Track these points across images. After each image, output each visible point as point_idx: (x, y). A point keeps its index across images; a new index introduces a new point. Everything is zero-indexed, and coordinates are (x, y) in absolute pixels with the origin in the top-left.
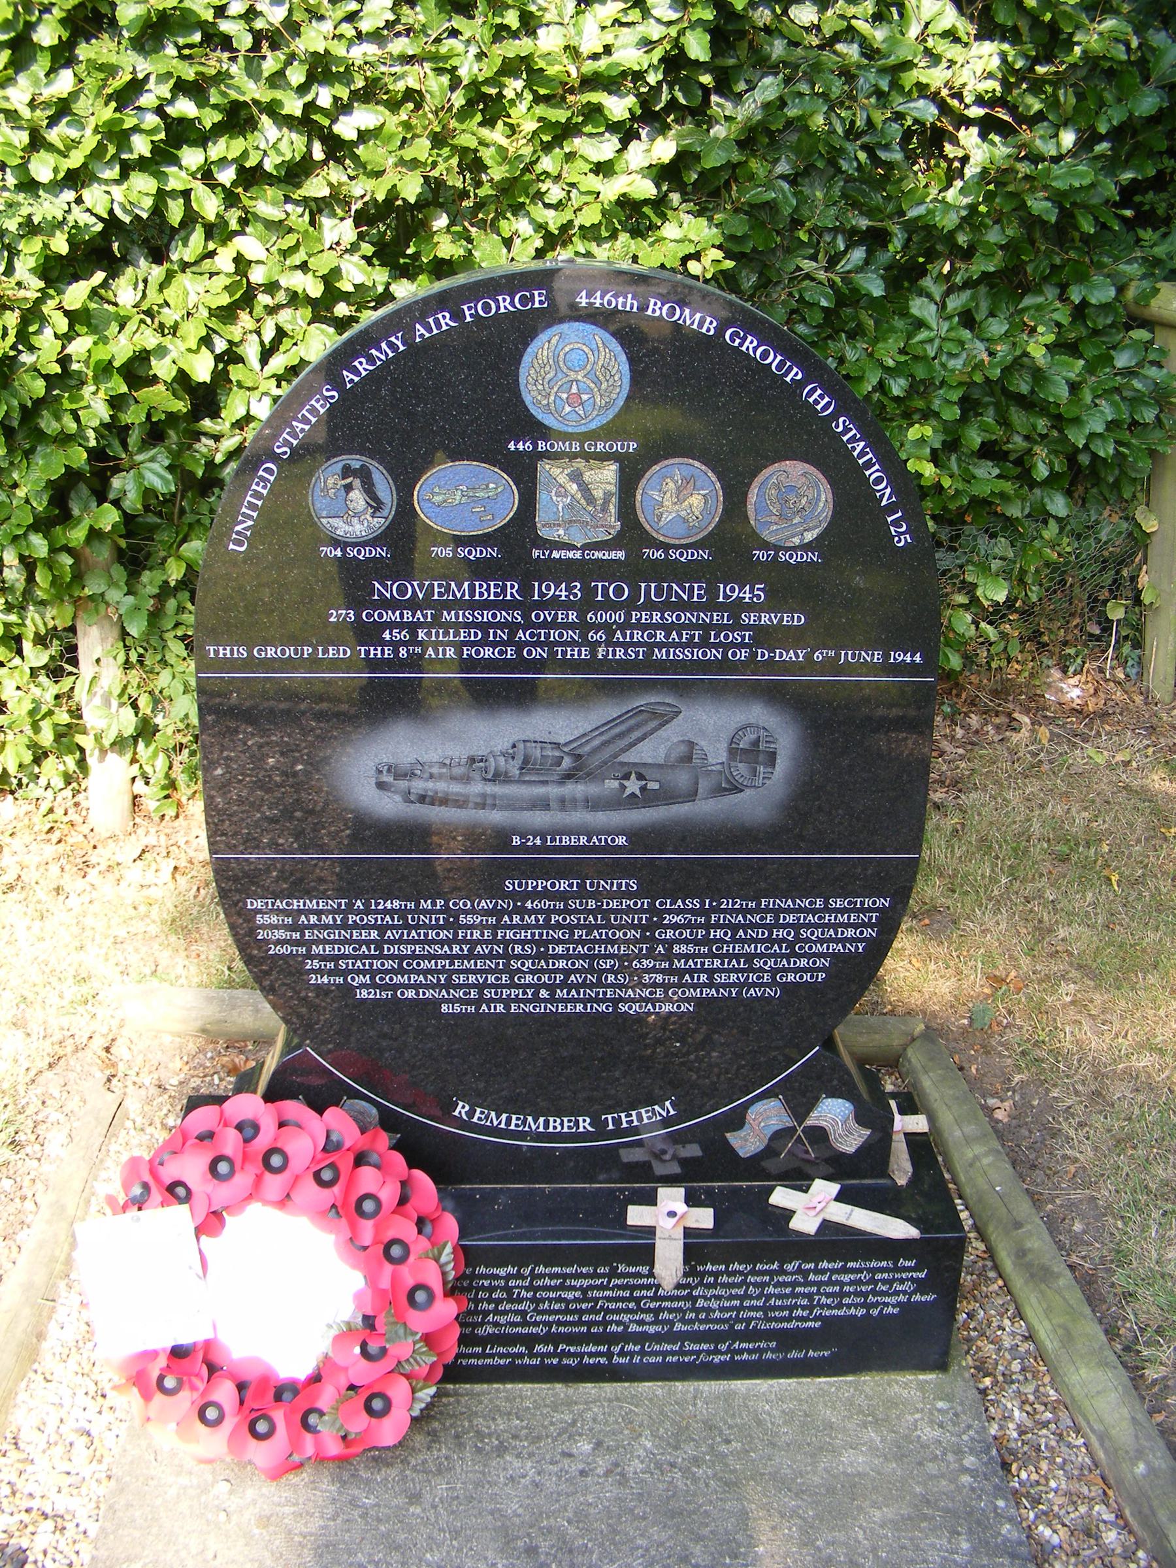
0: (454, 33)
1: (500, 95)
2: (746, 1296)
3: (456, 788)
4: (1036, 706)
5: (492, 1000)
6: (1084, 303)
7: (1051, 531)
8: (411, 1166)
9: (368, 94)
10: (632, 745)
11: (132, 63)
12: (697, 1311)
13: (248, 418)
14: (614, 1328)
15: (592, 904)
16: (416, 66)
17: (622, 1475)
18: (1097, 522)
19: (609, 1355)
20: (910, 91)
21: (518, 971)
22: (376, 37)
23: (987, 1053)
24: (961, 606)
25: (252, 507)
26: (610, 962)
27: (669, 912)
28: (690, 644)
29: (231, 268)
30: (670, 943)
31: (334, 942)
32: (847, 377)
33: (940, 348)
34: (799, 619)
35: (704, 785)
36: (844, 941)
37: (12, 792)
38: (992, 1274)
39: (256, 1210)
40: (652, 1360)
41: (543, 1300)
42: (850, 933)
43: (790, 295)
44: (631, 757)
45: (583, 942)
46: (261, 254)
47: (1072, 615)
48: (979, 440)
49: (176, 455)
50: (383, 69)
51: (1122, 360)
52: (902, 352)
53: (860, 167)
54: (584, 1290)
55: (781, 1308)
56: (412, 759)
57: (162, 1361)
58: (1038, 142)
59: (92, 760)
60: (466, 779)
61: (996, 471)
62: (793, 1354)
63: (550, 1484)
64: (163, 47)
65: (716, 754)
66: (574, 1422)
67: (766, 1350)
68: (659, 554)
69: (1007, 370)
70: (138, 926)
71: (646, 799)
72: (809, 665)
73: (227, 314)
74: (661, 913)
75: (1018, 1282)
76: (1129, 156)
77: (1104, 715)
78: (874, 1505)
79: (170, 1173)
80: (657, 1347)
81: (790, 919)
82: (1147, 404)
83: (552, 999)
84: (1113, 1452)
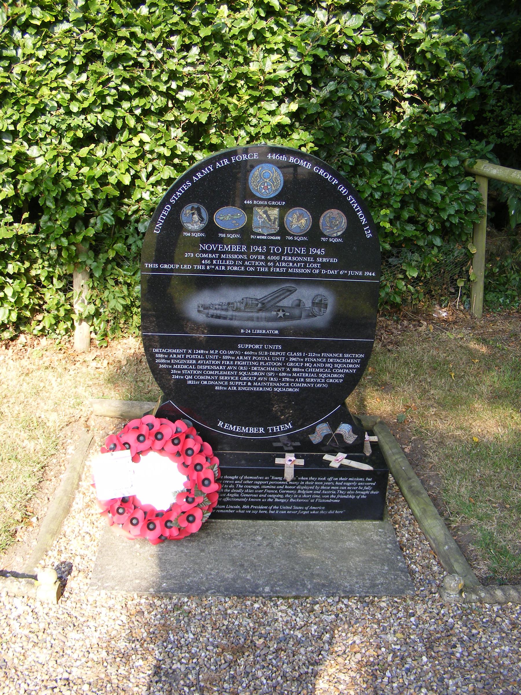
0: (220, 64)
1: (236, 86)
2: (315, 490)
3: (223, 313)
4: (429, 319)
5: (232, 385)
6: (447, 167)
7: (435, 251)
8: (204, 441)
9: (189, 85)
10: (281, 300)
11: (108, 72)
12: (298, 494)
13: (141, 199)
14: (270, 500)
15: (266, 353)
16: (206, 75)
17: (272, 546)
18: (453, 249)
19: (268, 510)
20: (384, 88)
21: (241, 376)
22: (193, 64)
23: (403, 431)
24: (401, 279)
25: (162, 219)
26: (272, 373)
27: (292, 357)
28: (300, 267)
29: (138, 144)
30: (291, 367)
31: (181, 364)
32: (359, 191)
33: (393, 182)
34: (335, 260)
35: (304, 314)
36: (349, 369)
37: (46, 336)
38: (400, 496)
39: (152, 455)
40: (283, 512)
41: (246, 489)
42: (351, 366)
43: (339, 161)
44: (280, 304)
45: (263, 366)
46: (149, 140)
47: (444, 284)
48: (408, 216)
49: (115, 211)
50: (194, 75)
51: (462, 188)
52: (379, 182)
53: (364, 115)
54: (260, 485)
55: (326, 494)
56: (209, 303)
57: (119, 503)
58: (430, 107)
59: (76, 324)
60: (227, 310)
61: (414, 228)
62: (330, 512)
63: (248, 548)
64: (118, 66)
65: (308, 304)
66: (256, 531)
67: (321, 510)
68: (291, 238)
69: (418, 190)
70: (96, 381)
71: (285, 318)
72: (338, 276)
73: (135, 161)
74: (289, 357)
75: (409, 496)
76: (466, 112)
77: (455, 323)
78: (357, 556)
79: (124, 439)
80: (284, 508)
81: (331, 360)
82: (472, 204)
83: (252, 386)
84: (438, 545)
